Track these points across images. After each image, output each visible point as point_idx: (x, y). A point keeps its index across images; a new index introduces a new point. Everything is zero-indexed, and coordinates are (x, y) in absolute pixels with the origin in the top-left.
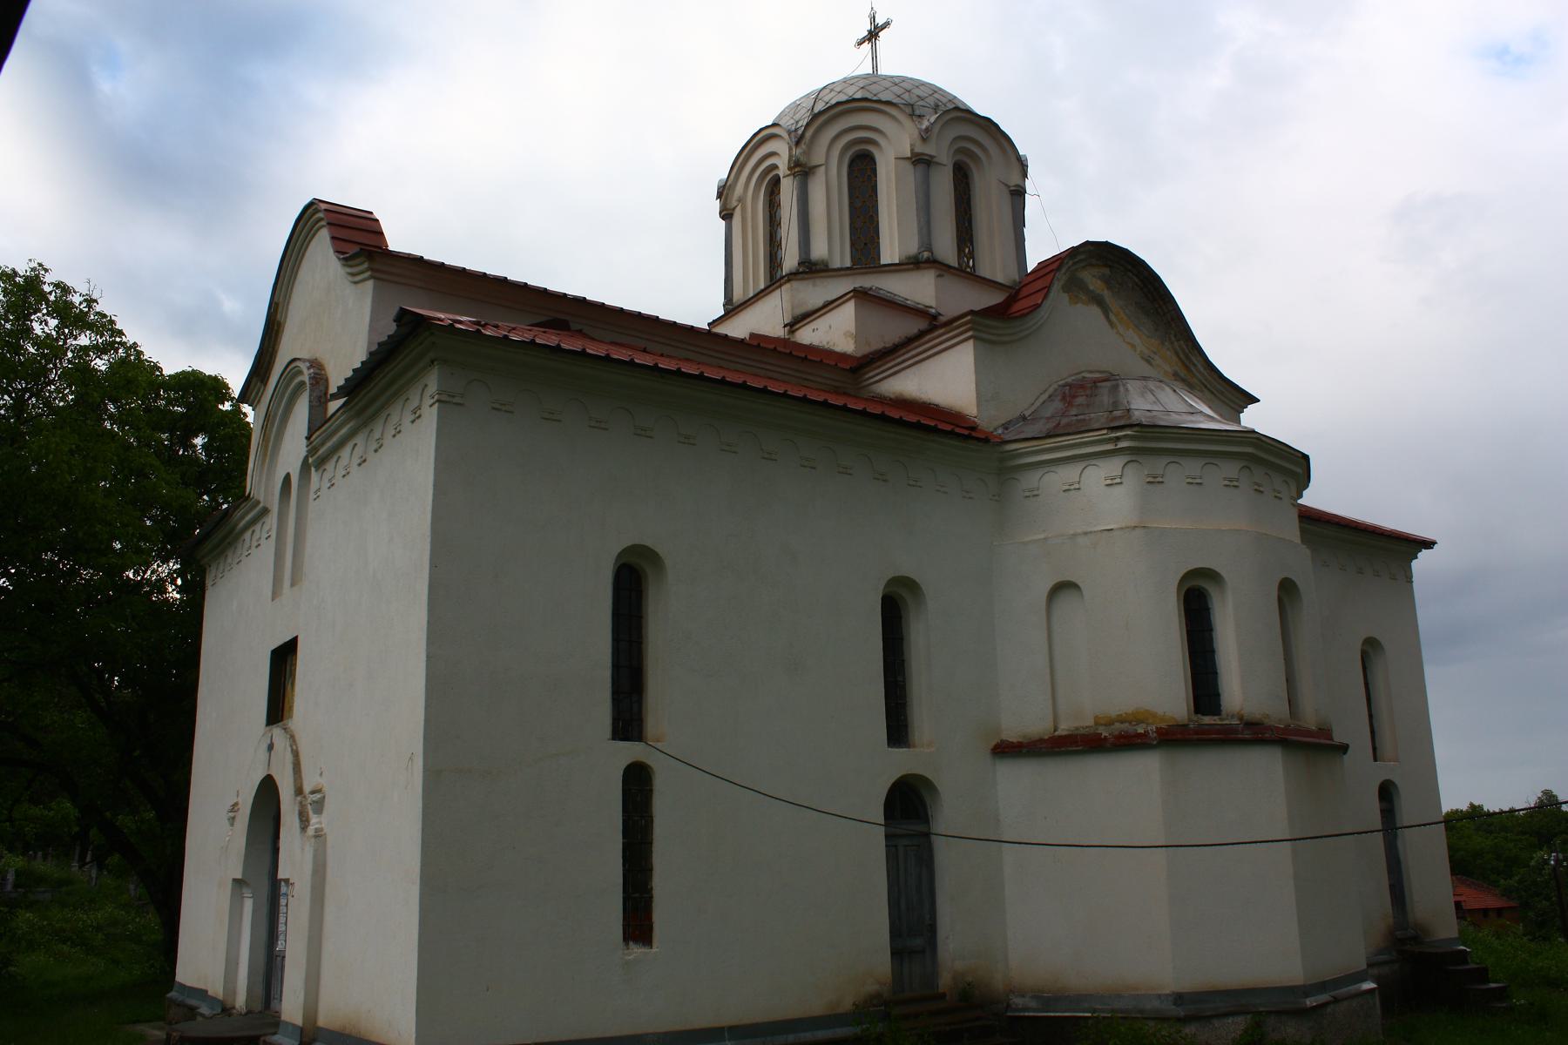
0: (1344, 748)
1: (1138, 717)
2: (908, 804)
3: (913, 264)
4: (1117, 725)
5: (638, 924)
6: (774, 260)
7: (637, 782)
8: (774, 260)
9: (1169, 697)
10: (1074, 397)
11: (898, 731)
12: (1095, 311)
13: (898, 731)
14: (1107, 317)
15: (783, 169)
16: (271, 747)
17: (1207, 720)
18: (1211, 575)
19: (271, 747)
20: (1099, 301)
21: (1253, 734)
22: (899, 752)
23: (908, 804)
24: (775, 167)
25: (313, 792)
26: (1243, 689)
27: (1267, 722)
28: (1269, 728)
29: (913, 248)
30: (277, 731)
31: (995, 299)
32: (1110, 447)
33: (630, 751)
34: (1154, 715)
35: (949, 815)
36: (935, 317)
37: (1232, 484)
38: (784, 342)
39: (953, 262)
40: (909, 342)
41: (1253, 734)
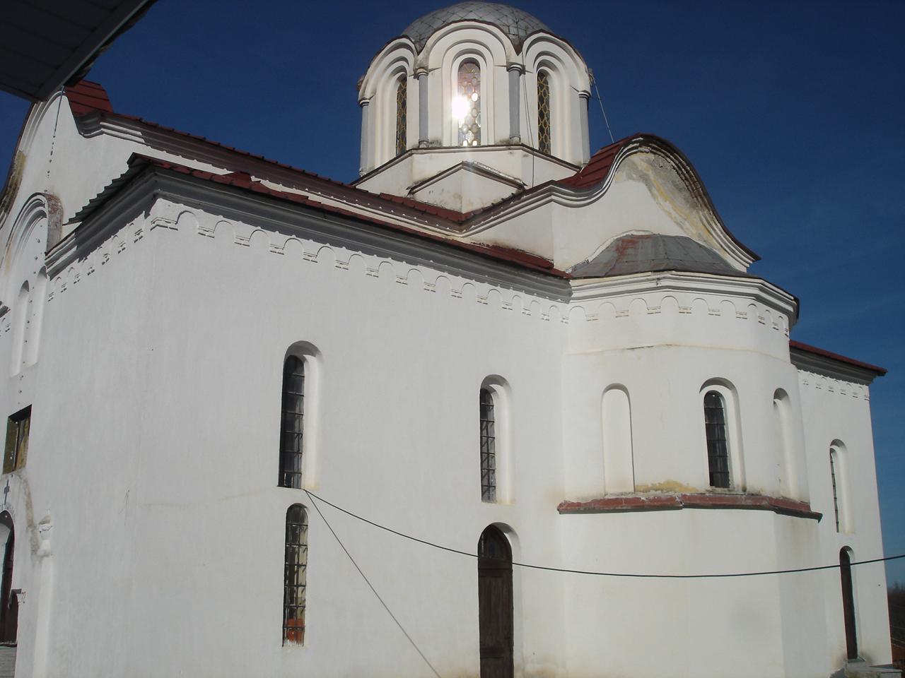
0: (818, 517)
1: (669, 486)
2: (495, 551)
3: (508, 145)
4: (653, 492)
5: (293, 628)
6: (401, 136)
7: (296, 516)
8: (401, 136)
9: (697, 476)
10: (625, 248)
11: (488, 489)
12: (642, 186)
13: (488, 489)
14: (650, 191)
15: (410, 70)
16: (7, 490)
17: (719, 490)
18: (310, 349)
19: (7, 490)
20: (644, 178)
21: (756, 502)
22: (487, 506)
23: (495, 551)
24: (403, 69)
25: (43, 523)
26: (747, 469)
27: (764, 494)
28: (764, 498)
29: (505, 134)
30: (13, 480)
31: (571, 173)
32: (653, 285)
33: (291, 496)
34: (680, 486)
35: (523, 550)
36: (520, 186)
37: (742, 316)
38: (406, 199)
39: (537, 147)
40: (505, 203)
41: (756, 502)
